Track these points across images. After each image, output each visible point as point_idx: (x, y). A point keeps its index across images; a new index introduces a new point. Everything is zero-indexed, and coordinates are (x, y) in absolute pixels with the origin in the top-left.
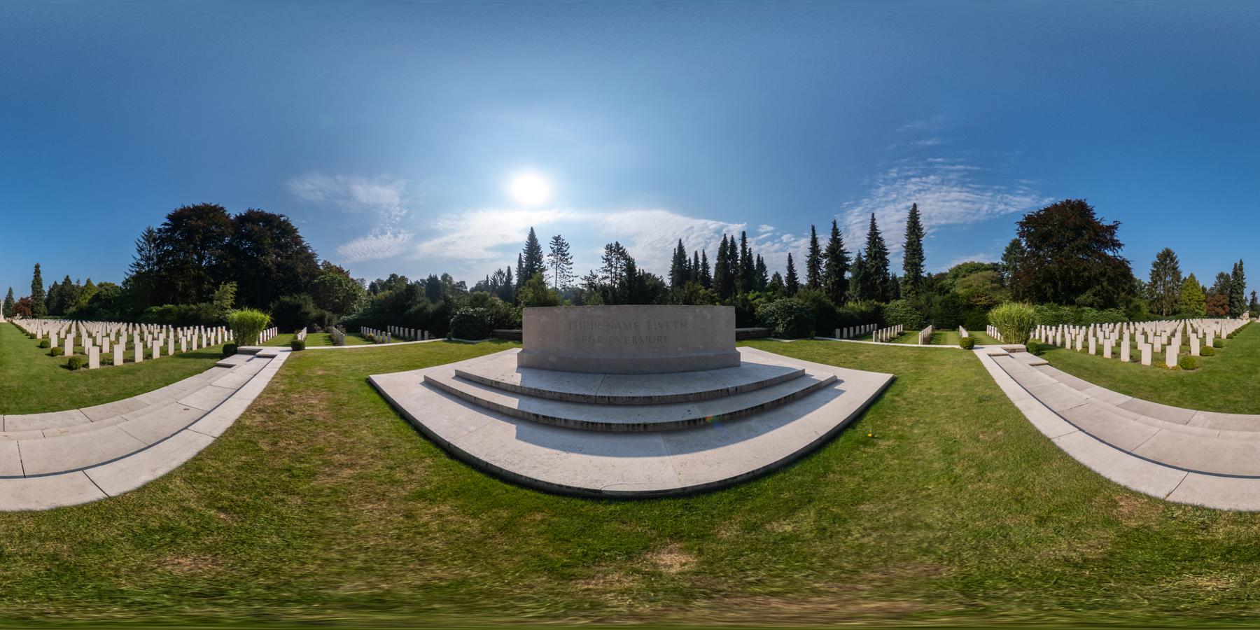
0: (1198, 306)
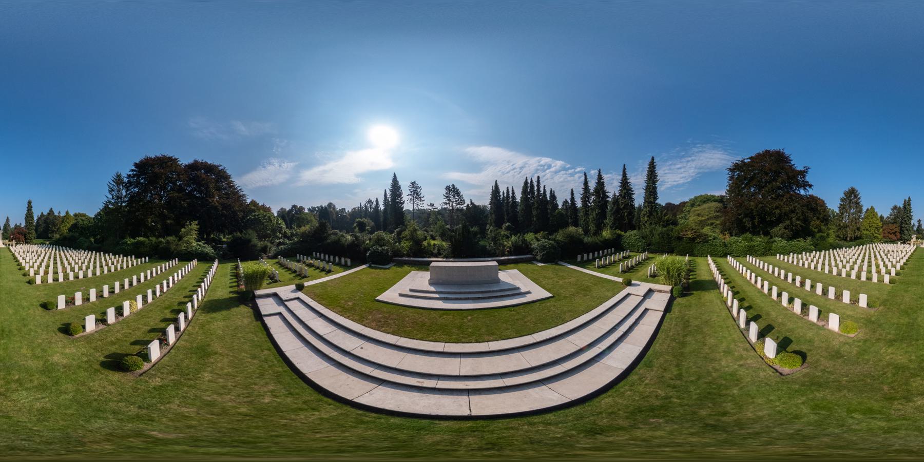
0: (876, 232)
